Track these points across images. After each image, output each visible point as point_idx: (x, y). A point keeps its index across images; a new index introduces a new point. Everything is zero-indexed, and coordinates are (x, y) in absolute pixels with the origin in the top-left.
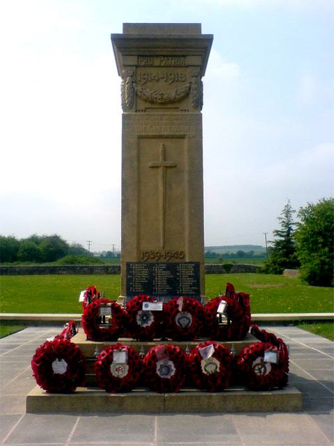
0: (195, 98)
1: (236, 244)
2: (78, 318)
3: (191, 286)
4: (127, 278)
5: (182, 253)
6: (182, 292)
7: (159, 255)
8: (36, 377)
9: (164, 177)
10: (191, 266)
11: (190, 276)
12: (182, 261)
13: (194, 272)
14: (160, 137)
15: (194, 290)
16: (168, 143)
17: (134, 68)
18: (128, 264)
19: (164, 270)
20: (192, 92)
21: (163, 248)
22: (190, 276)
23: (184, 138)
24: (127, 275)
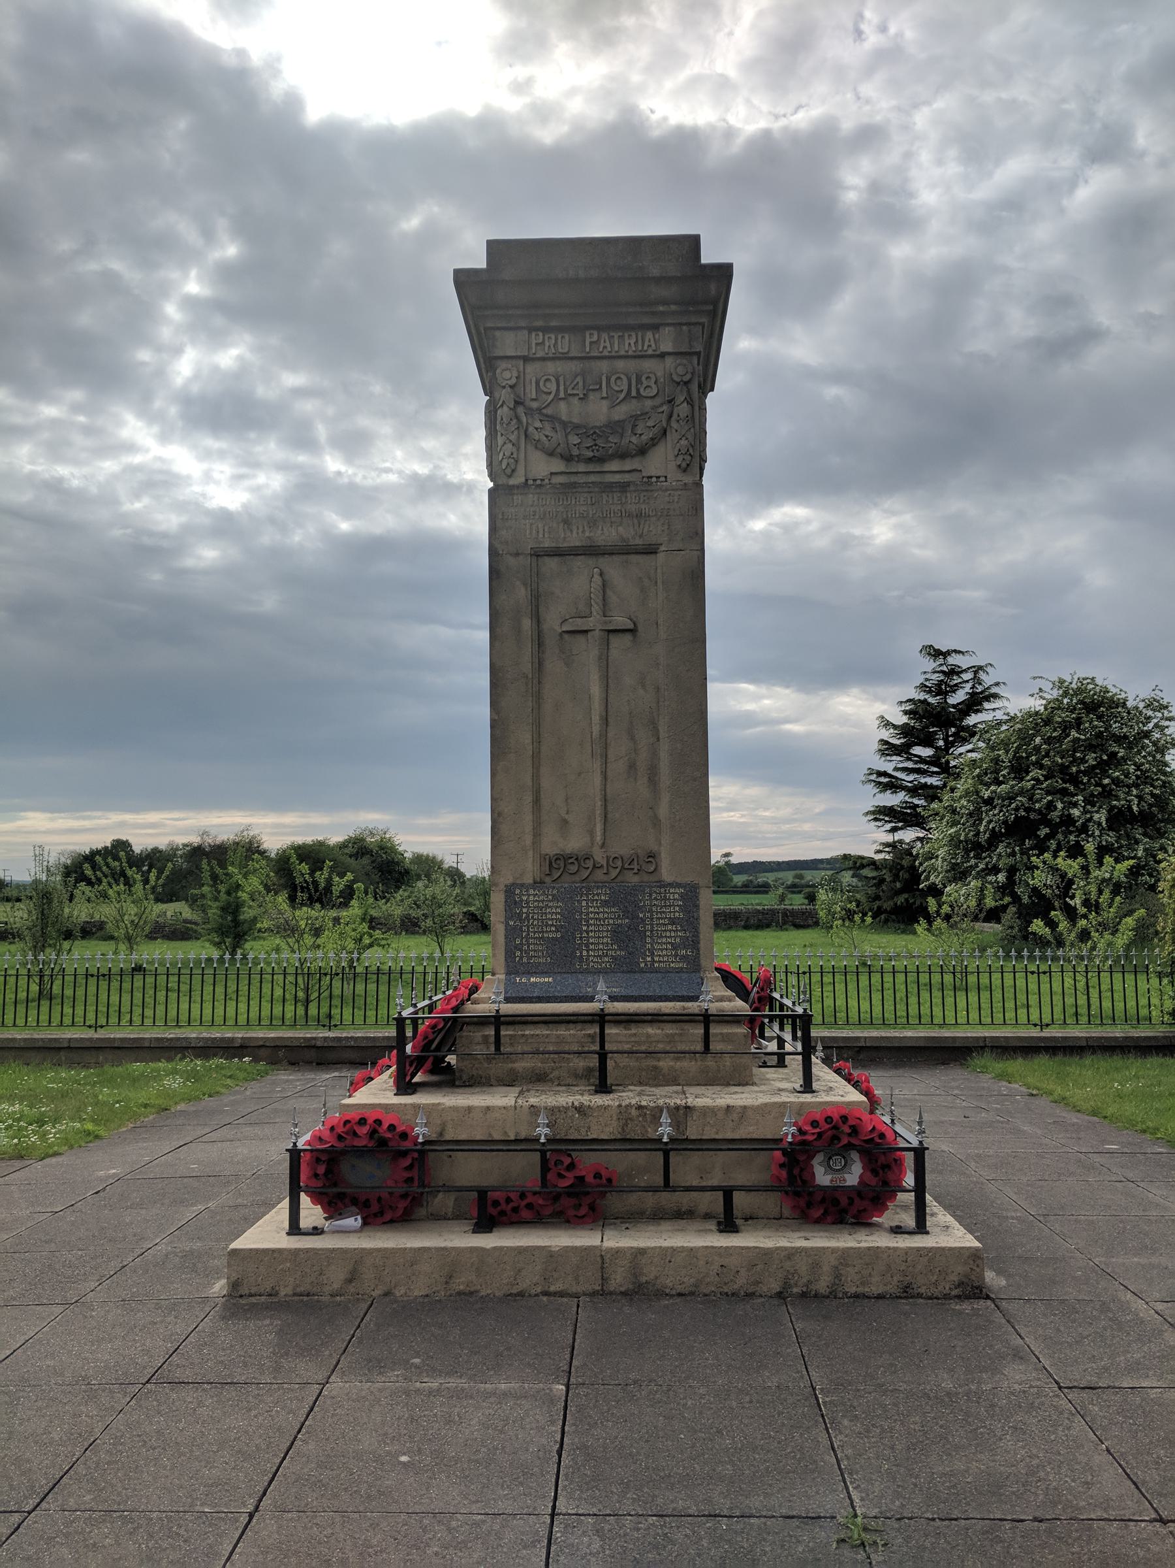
0: (684, 442)
1: (805, 931)
2: (388, 1038)
3: (675, 947)
4: (507, 924)
5: (652, 856)
6: (653, 961)
7: (590, 864)
8: (231, 61)
9: (605, 662)
10: (675, 894)
11: (673, 922)
12: (653, 878)
13: (683, 909)
14: (591, 551)
15: (684, 958)
16: (613, 568)
17: (526, 332)
18: (509, 891)
19: (605, 904)
20: (674, 425)
21: (603, 846)
22: (673, 922)
23: (707, 1214)
24: (507, 919)
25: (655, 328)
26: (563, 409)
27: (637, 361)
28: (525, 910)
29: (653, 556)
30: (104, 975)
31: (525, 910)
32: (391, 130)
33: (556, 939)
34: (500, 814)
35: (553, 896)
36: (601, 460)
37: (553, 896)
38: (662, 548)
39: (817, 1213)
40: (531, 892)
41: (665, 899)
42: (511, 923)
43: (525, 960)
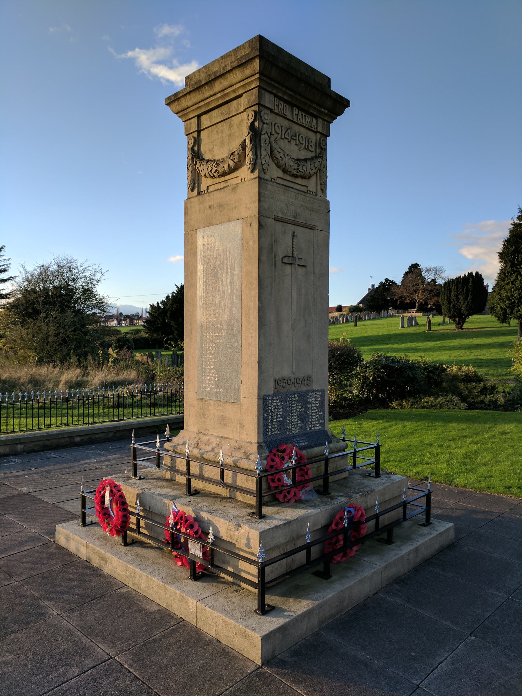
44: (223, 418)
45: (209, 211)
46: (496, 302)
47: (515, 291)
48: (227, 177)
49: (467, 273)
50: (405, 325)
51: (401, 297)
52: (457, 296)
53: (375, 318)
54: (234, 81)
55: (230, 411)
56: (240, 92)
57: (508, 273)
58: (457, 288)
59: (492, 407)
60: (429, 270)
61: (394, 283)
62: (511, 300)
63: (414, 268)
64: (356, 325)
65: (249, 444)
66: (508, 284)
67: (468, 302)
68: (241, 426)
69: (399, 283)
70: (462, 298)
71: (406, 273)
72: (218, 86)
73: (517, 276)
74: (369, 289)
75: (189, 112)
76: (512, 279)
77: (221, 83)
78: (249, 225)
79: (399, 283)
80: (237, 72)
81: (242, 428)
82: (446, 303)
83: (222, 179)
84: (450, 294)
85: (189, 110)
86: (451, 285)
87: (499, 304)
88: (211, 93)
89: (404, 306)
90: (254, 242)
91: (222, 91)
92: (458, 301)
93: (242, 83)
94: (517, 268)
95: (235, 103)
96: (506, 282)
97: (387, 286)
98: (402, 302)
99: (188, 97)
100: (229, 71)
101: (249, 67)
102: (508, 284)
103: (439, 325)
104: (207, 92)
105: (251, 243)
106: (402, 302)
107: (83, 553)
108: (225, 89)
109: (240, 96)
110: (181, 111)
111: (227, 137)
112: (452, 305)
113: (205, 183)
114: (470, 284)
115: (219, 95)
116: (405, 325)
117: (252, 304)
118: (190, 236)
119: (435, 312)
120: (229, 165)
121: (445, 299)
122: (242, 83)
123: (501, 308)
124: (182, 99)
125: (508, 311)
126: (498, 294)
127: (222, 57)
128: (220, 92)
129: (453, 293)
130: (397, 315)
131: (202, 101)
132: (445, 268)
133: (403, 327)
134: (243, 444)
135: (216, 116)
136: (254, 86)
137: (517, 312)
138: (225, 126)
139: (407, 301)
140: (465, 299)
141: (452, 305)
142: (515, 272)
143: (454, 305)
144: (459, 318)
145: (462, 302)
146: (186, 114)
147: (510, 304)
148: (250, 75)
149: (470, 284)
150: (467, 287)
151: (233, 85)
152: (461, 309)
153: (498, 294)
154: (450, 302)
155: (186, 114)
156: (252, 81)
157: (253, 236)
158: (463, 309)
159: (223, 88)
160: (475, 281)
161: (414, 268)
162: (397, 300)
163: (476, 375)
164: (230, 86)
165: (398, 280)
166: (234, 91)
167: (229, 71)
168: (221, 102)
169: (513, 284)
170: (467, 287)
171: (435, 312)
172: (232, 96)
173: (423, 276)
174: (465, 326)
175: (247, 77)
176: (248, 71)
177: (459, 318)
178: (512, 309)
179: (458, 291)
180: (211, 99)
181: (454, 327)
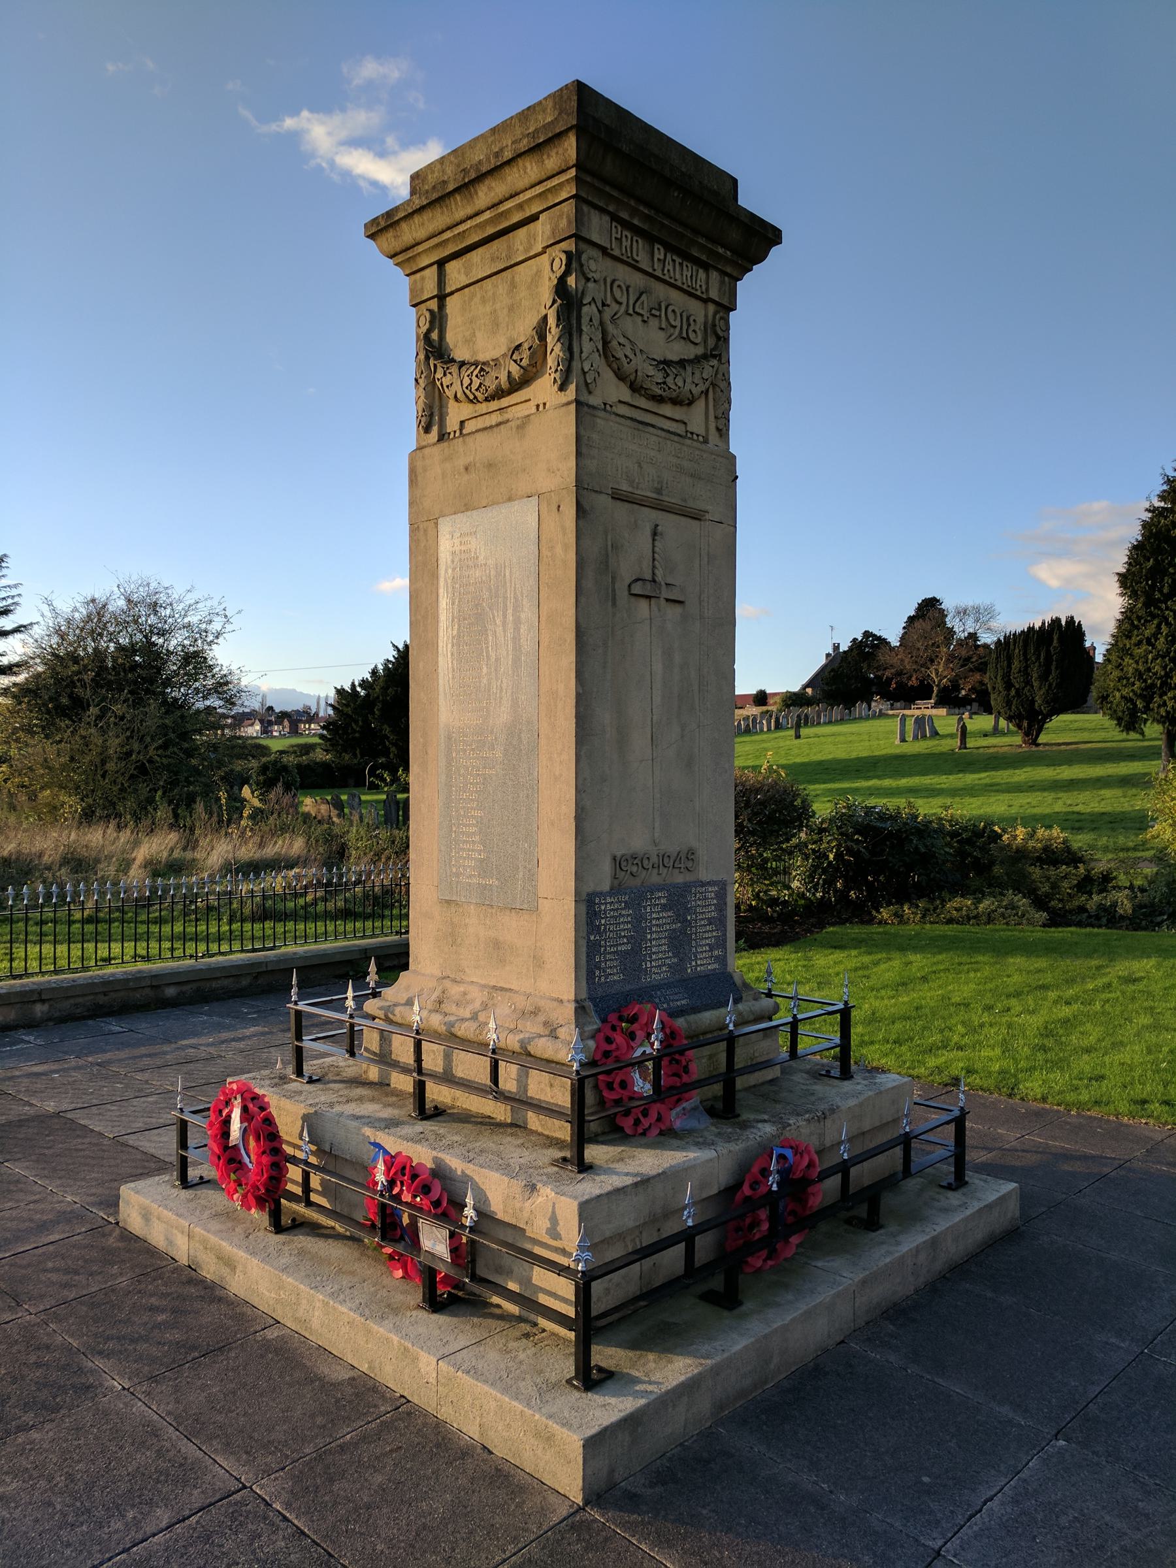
19: (664, 908)
25: (706, 267)
26: (330, 906)
27: (687, 298)
28: (603, 922)
29: (697, 522)
30: (191, 939)
31: (603, 922)
32: (1031, 766)
33: (626, 952)
34: (583, 809)
35: (626, 902)
36: (660, 400)
37: (626, 902)
38: (707, 516)
39: (723, 385)
40: (609, 900)
41: (706, 898)
42: (592, 938)
43: (603, 979)
44: (497, 944)
45: (466, 477)
46: (1112, 684)
47: (1155, 659)
48: (505, 402)
49: (1048, 620)
50: (909, 737)
51: (900, 673)
52: (1025, 672)
53: (842, 721)
54: (521, 185)
55: (512, 928)
56: (535, 209)
57: (1139, 618)
58: (1025, 654)
59: (1104, 920)
60: (963, 613)
61: (883, 641)
62: (1145, 681)
63: (929, 609)
64: (798, 736)
65: (555, 1004)
66: (1139, 644)
67: (1050, 685)
68: (538, 962)
69: (894, 641)
70: (1035, 675)
71: (911, 620)
72: (484, 195)
73: (1159, 627)
74: (828, 655)
75: (419, 254)
76: (1147, 633)
77: (490, 188)
78: (555, 508)
79: (894, 641)
80: (528, 165)
81: (539, 966)
82: (1000, 685)
83: (494, 405)
84: (1009, 666)
85: (420, 248)
86: (1012, 647)
87: (1119, 690)
88: (470, 211)
89: (907, 695)
90: (566, 547)
91: (493, 207)
92: (1028, 683)
93: (539, 189)
94: (1160, 609)
95: (522, 233)
96: (1134, 640)
97: (868, 647)
98: (901, 685)
99: (417, 219)
100: (509, 162)
101: (553, 153)
102: (1139, 644)
103: (985, 735)
104: (460, 209)
105: (559, 550)
106: (901, 685)
107: (182, 1250)
108: (501, 202)
109: (534, 218)
110: (401, 252)
111: (505, 311)
112: (1013, 692)
113: (456, 413)
114: (1055, 643)
115: (487, 215)
116: (909, 737)
117: (561, 687)
118: (422, 532)
119: (975, 705)
120: (509, 372)
121: (999, 678)
122: (539, 189)
123: (1122, 697)
124: (404, 225)
125: (1140, 704)
126: (1117, 667)
127: (493, 131)
128: (489, 209)
129: (1016, 665)
130: (891, 712)
131: (449, 228)
132: (998, 608)
133: (903, 740)
134: (542, 1003)
135: (480, 262)
136: (564, 195)
137: (1159, 706)
138: (499, 286)
139: (914, 682)
140: (1044, 677)
141: (1013, 692)
142: (1154, 616)
143: (1017, 690)
144: (1030, 721)
145: (1036, 684)
146: (413, 258)
147: (1142, 689)
148: (557, 169)
149: (1055, 643)
150: (1048, 651)
151: (517, 194)
152: (1033, 701)
153: (1117, 667)
154: (1009, 685)
155: (413, 258)
156: (561, 185)
157: (563, 529)
158: (1039, 700)
159: (496, 200)
160: (1064, 637)
161: (929, 609)
162: (889, 680)
163: (1068, 850)
164: (512, 196)
165: (894, 639)
166: (520, 206)
167: (509, 162)
168: (491, 230)
169: (1149, 643)
170: (1048, 651)
171: (975, 705)
172: (516, 218)
173: (949, 625)
174: (1042, 739)
175: (549, 174)
176: (552, 162)
177: (1030, 721)
178: (1148, 700)
179: (1026, 660)
180: (469, 224)
181: (1018, 739)
